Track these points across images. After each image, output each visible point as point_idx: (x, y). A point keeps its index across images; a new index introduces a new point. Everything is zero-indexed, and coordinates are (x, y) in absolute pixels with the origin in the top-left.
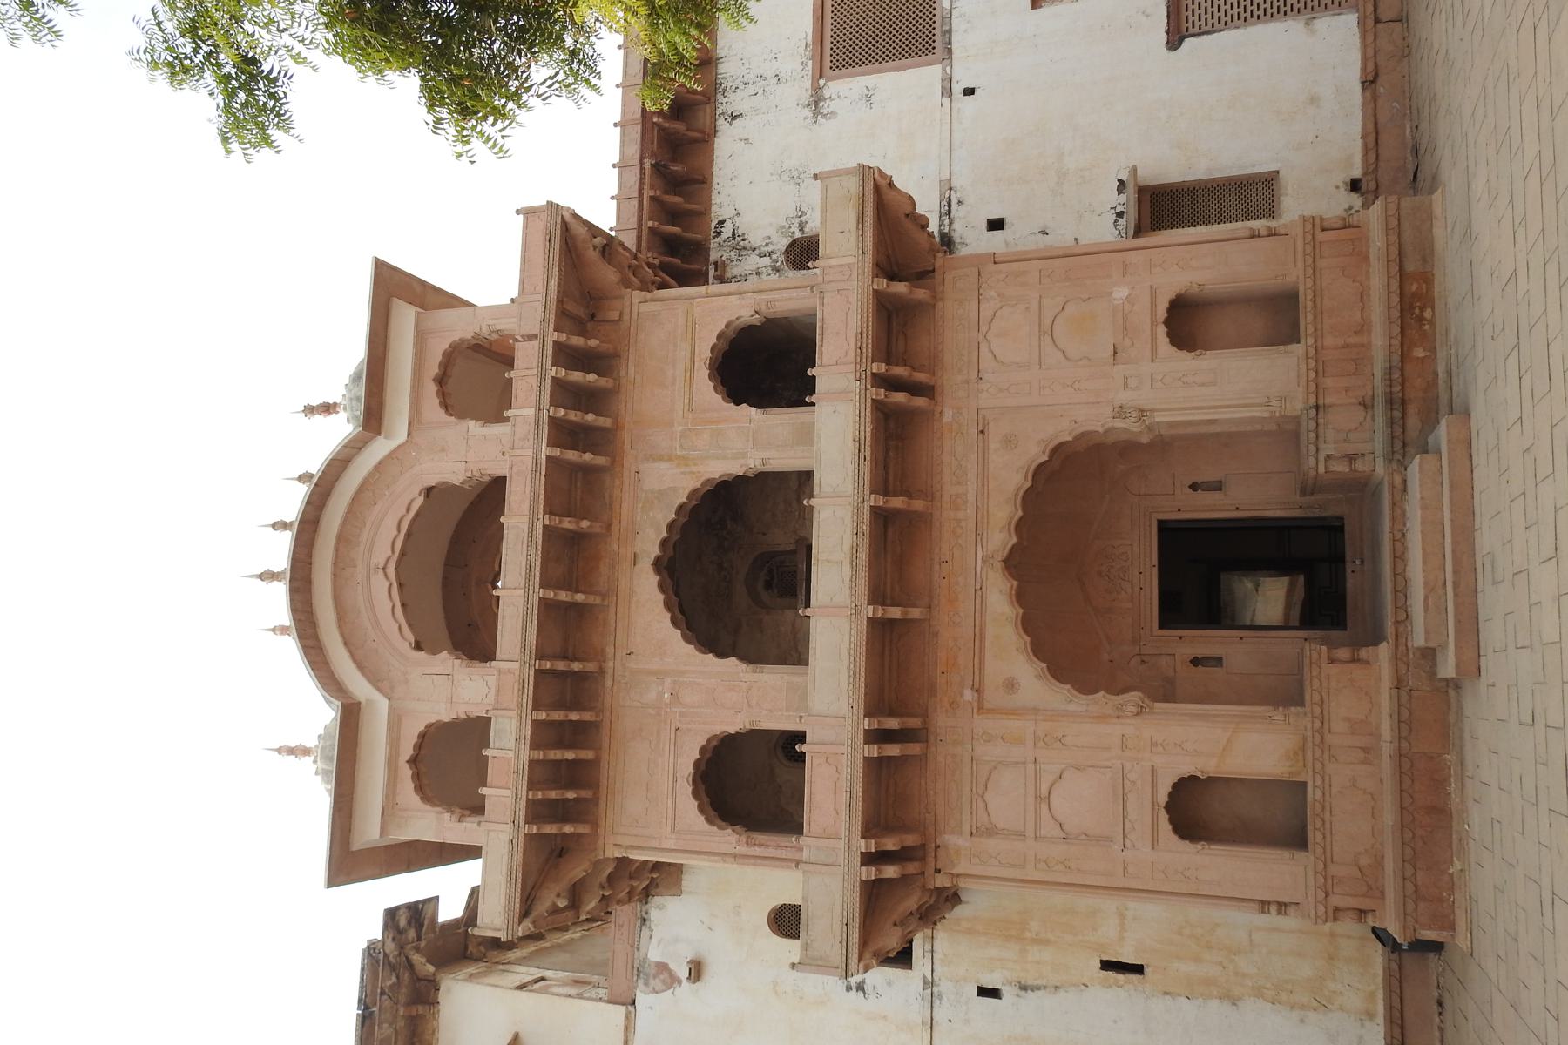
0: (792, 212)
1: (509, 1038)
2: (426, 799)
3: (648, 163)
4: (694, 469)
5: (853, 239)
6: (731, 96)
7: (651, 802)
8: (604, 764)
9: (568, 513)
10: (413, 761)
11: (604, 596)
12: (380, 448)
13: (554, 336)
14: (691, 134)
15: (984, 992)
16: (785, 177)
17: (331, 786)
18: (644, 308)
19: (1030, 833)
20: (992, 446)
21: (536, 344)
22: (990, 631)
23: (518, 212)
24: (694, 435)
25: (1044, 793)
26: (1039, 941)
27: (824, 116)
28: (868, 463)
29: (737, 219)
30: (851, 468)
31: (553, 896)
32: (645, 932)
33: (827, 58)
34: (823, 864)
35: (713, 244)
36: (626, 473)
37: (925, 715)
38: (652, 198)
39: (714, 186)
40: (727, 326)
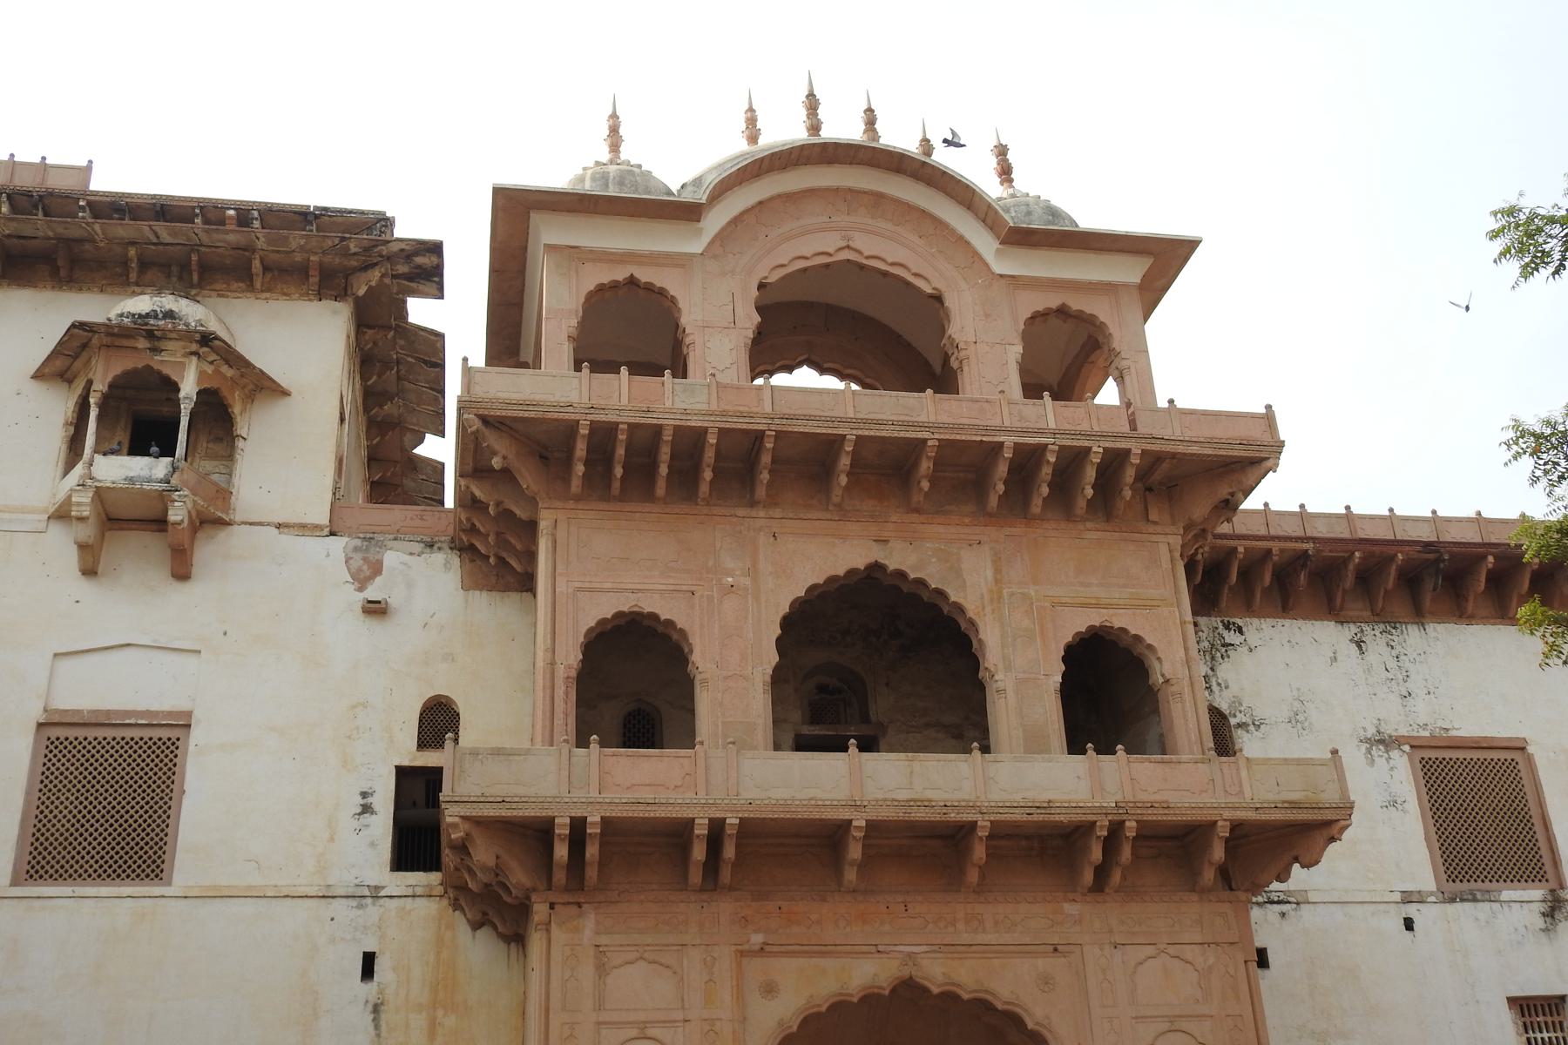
0: (1258, 714)
1: (284, 383)
2: (590, 296)
3: (1309, 546)
4: (988, 610)
5: (1271, 797)
6: (1382, 640)
7: (600, 565)
8: (648, 507)
9: (938, 463)
10: (632, 281)
11: (839, 506)
12: (985, 243)
13: (1136, 451)
14: (1340, 594)
15: (369, 961)
16: (1297, 704)
17: (588, 187)
18: (1164, 549)
19: (605, 1017)
20: (1040, 962)
21: (1126, 429)
22: (829, 963)
23: (1269, 407)
24: (1022, 604)
25: (652, 1032)
26: (432, 1028)
27: (1369, 751)
28: (1025, 818)
29: (1245, 649)
30: (1017, 798)
31: (504, 452)
32: (418, 547)
33: (1433, 754)
34: (523, 757)
35: (1216, 621)
36: (978, 529)
37: (731, 889)
38: (1269, 552)
39: (1281, 622)
40: (1150, 647)
